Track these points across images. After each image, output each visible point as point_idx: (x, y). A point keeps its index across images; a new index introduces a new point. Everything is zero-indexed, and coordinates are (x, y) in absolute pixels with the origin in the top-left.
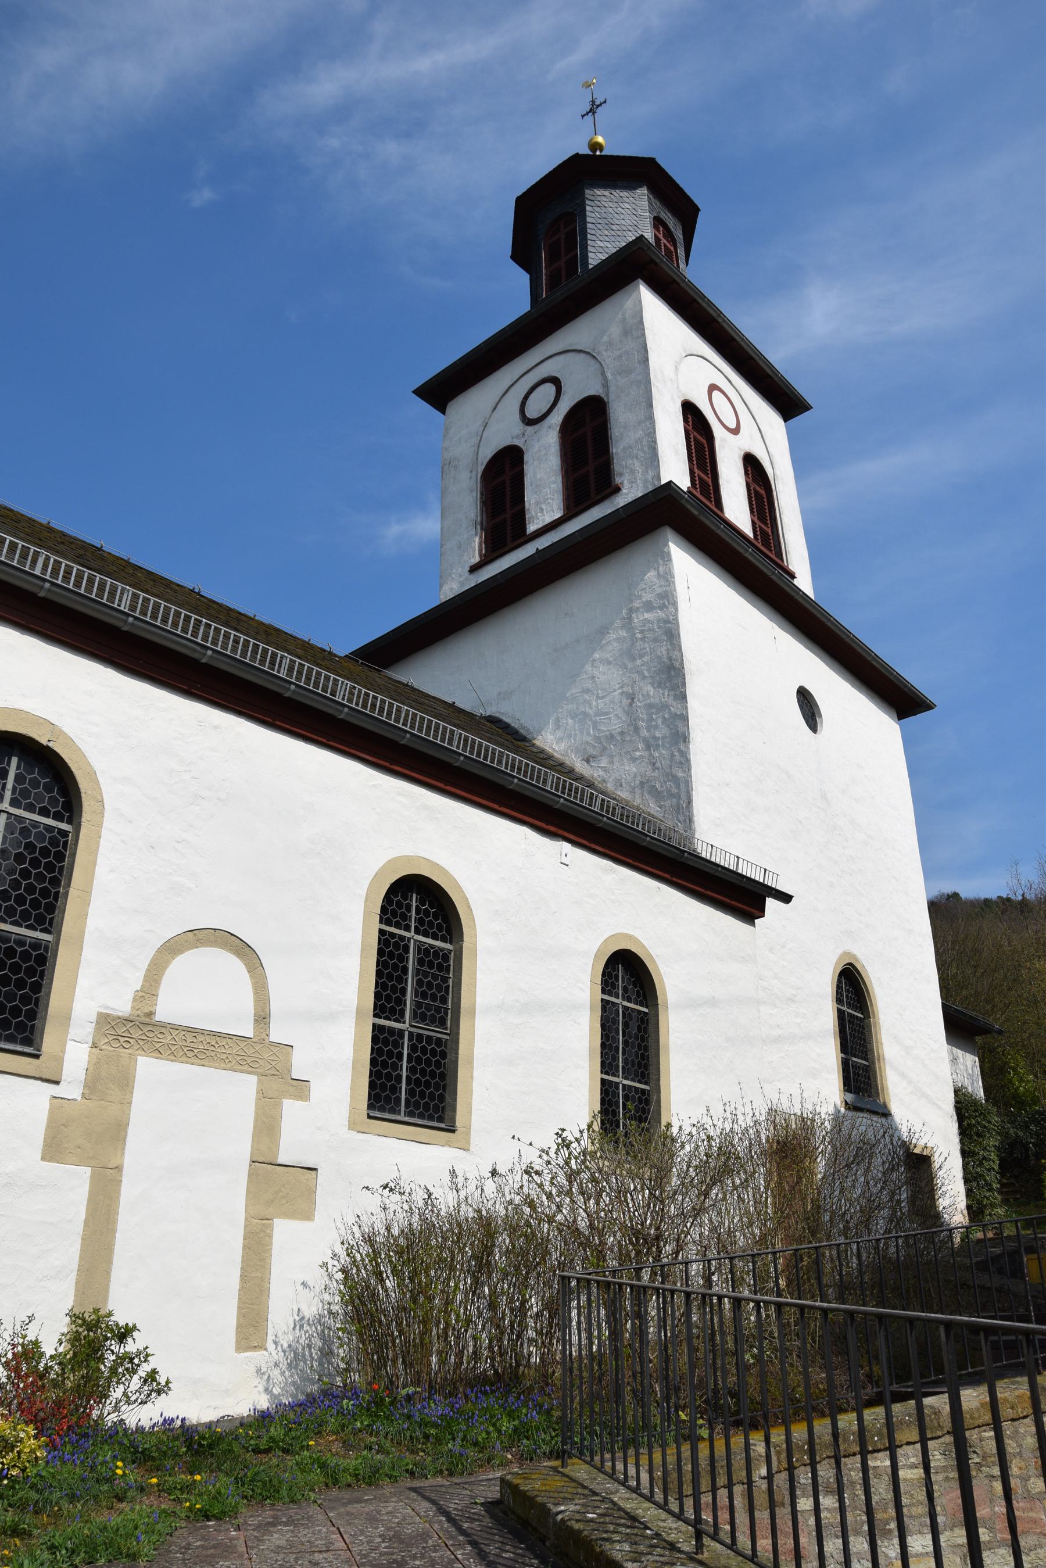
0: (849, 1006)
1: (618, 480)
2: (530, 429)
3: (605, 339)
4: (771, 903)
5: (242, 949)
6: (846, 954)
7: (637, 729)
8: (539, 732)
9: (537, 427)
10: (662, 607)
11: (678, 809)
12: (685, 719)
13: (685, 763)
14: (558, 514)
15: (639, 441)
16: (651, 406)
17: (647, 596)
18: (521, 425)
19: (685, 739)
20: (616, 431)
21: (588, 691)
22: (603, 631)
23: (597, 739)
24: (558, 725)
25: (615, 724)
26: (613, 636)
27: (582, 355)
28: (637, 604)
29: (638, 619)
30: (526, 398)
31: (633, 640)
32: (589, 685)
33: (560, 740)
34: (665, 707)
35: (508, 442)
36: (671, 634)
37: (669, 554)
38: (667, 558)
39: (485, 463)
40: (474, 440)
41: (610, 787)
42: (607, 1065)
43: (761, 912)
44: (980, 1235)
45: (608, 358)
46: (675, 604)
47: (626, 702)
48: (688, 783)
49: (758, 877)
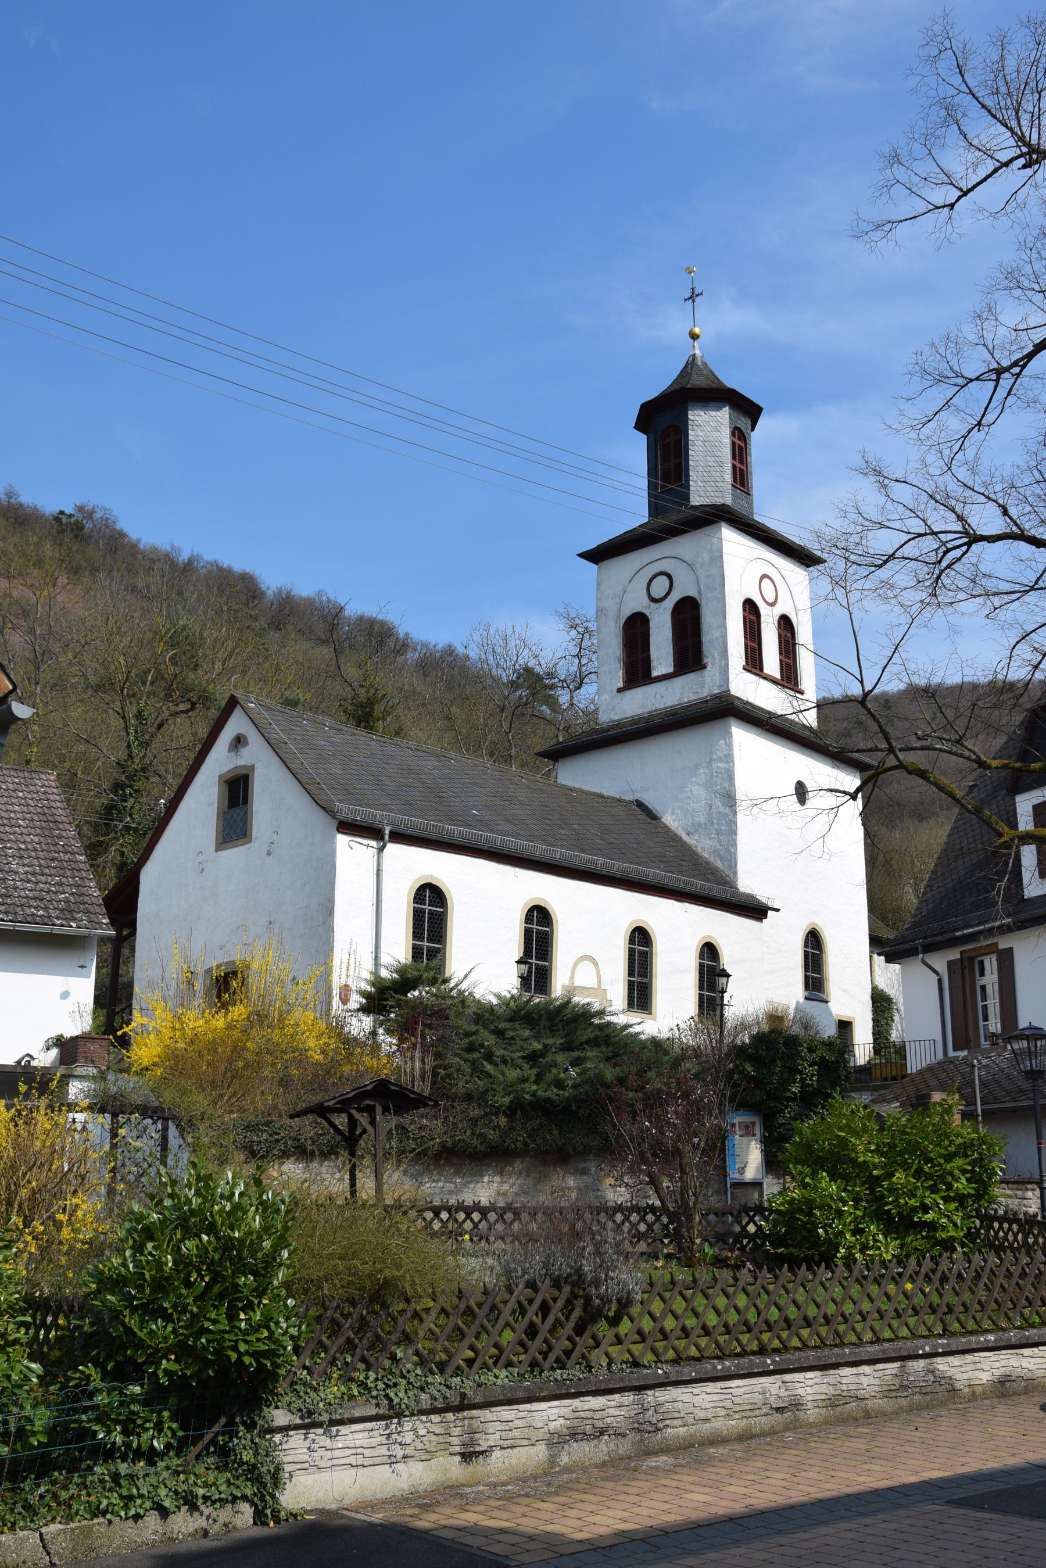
0: (812, 948)
1: (705, 660)
2: (653, 605)
3: (700, 559)
4: (770, 913)
5: (595, 963)
6: (812, 923)
7: (712, 824)
8: (664, 814)
9: (657, 605)
10: (727, 762)
11: (731, 867)
12: (735, 823)
13: (735, 845)
14: (671, 670)
15: (717, 638)
16: (725, 618)
17: (719, 754)
18: (648, 600)
19: (735, 833)
20: (705, 628)
21: (689, 798)
22: (697, 767)
23: (693, 824)
24: (673, 813)
25: (702, 819)
26: (702, 771)
27: (685, 565)
28: (714, 757)
29: (715, 765)
30: (651, 581)
31: (712, 777)
32: (689, 794)
33: (675, 821)
34: (726, 815)
35: (639, 609)
36: (730, 777)
37: (731, 733)
38: (730, 735)
39: (626, 617)
40: (618, 600)
41: (699, 850)
42: (701, 988)
43: (765, 916)
44: (877, 1061)
45: (702, 573)
46: (733, 762)
47: (708, 808)
48: (735, 855)
49: (765, 901)
